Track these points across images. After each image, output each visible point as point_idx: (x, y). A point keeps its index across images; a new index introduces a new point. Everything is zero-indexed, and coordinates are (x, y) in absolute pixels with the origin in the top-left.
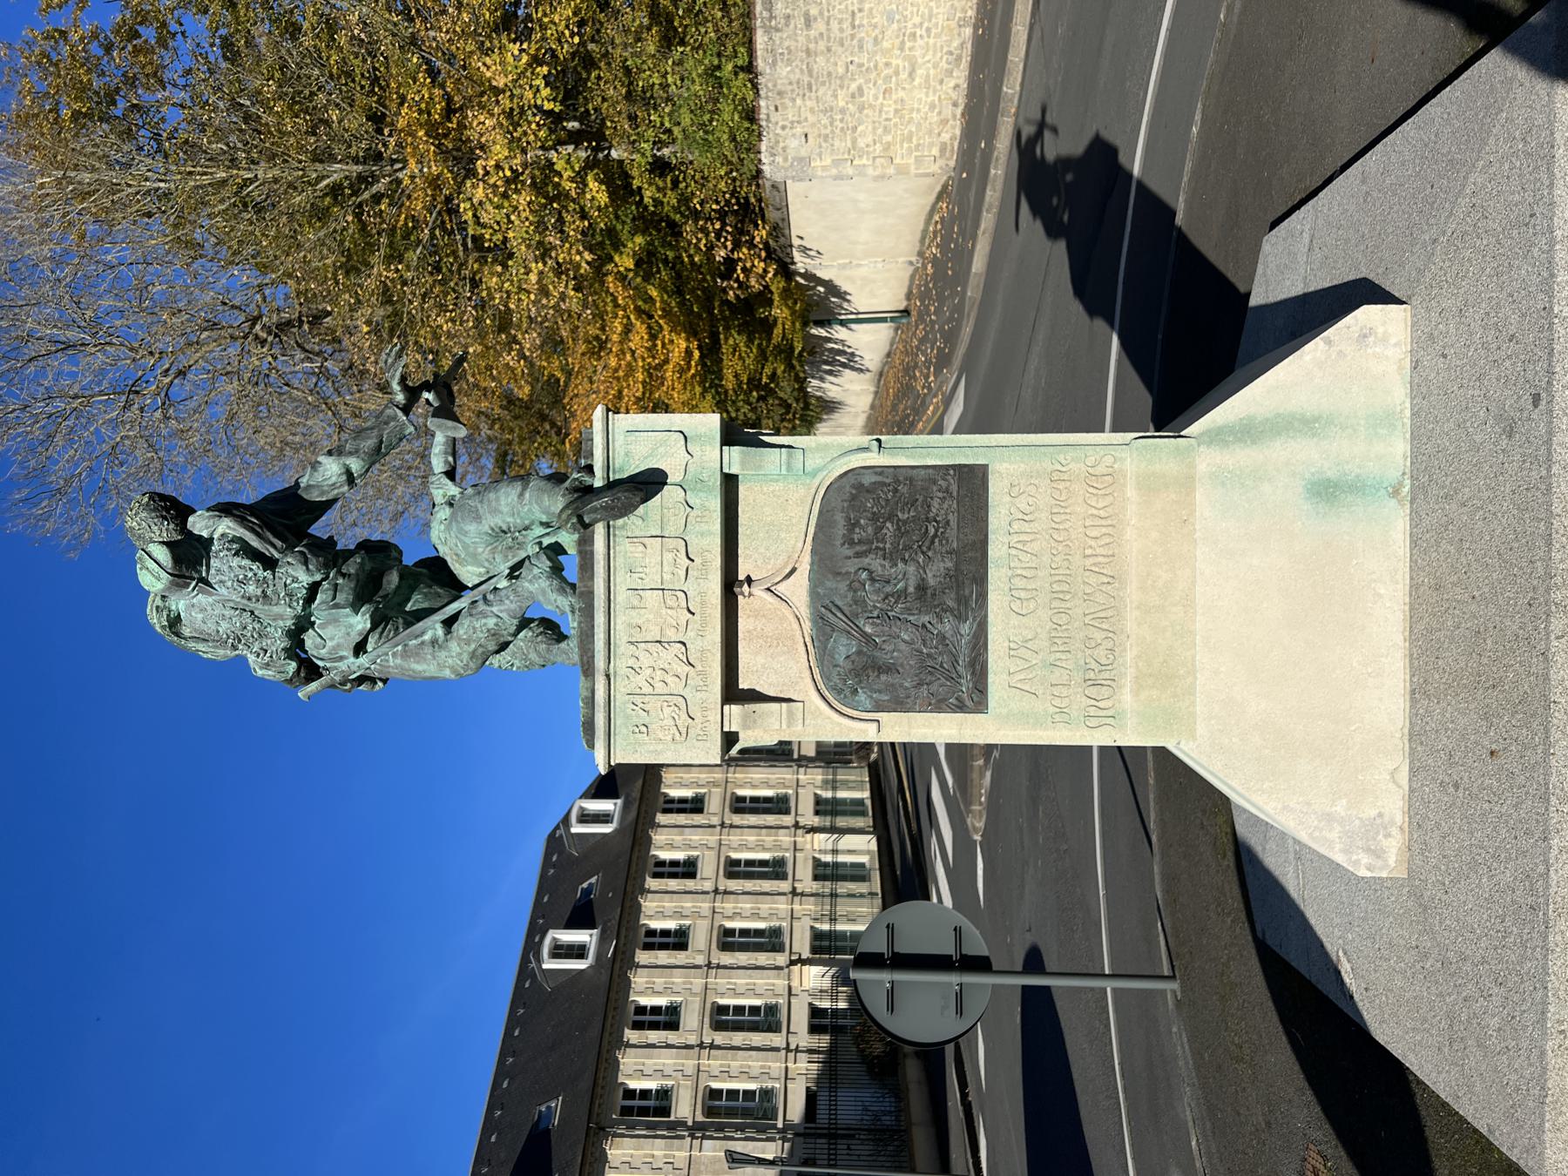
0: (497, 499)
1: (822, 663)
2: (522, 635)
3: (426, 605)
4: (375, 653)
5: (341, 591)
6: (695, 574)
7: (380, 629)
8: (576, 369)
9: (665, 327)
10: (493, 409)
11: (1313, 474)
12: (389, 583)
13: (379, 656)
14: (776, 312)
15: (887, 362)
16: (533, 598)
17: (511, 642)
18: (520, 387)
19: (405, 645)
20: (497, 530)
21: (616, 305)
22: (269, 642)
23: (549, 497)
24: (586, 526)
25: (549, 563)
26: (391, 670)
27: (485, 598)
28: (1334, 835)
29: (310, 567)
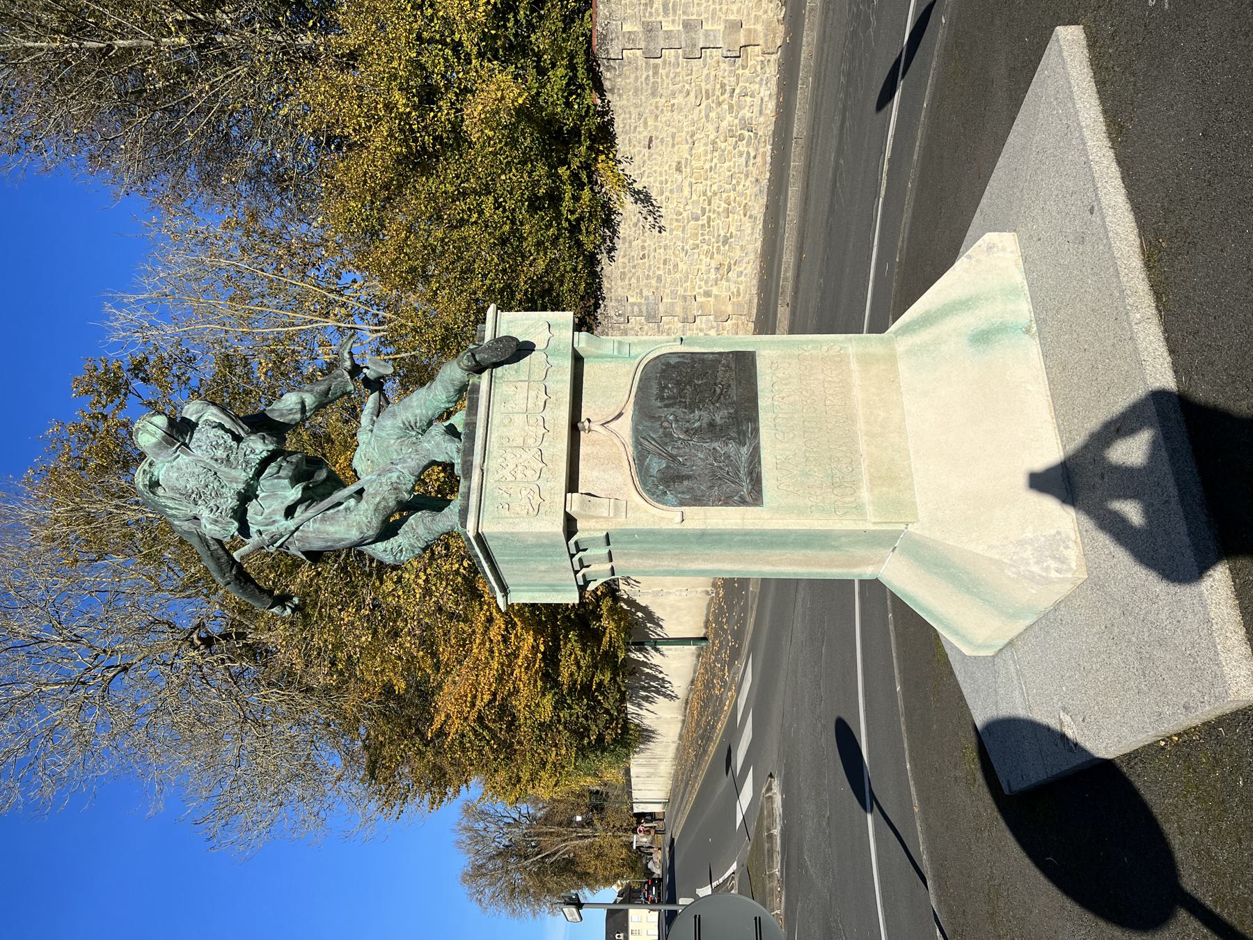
1: (640, 473)
5: (284, 469)
9: (519, 623)
11: (972, 331)
12: (319, 476)
14: (604, 623)
15: (691, 689)
22: (222, 501)
26: (309, 535)
28: (1029, 552)
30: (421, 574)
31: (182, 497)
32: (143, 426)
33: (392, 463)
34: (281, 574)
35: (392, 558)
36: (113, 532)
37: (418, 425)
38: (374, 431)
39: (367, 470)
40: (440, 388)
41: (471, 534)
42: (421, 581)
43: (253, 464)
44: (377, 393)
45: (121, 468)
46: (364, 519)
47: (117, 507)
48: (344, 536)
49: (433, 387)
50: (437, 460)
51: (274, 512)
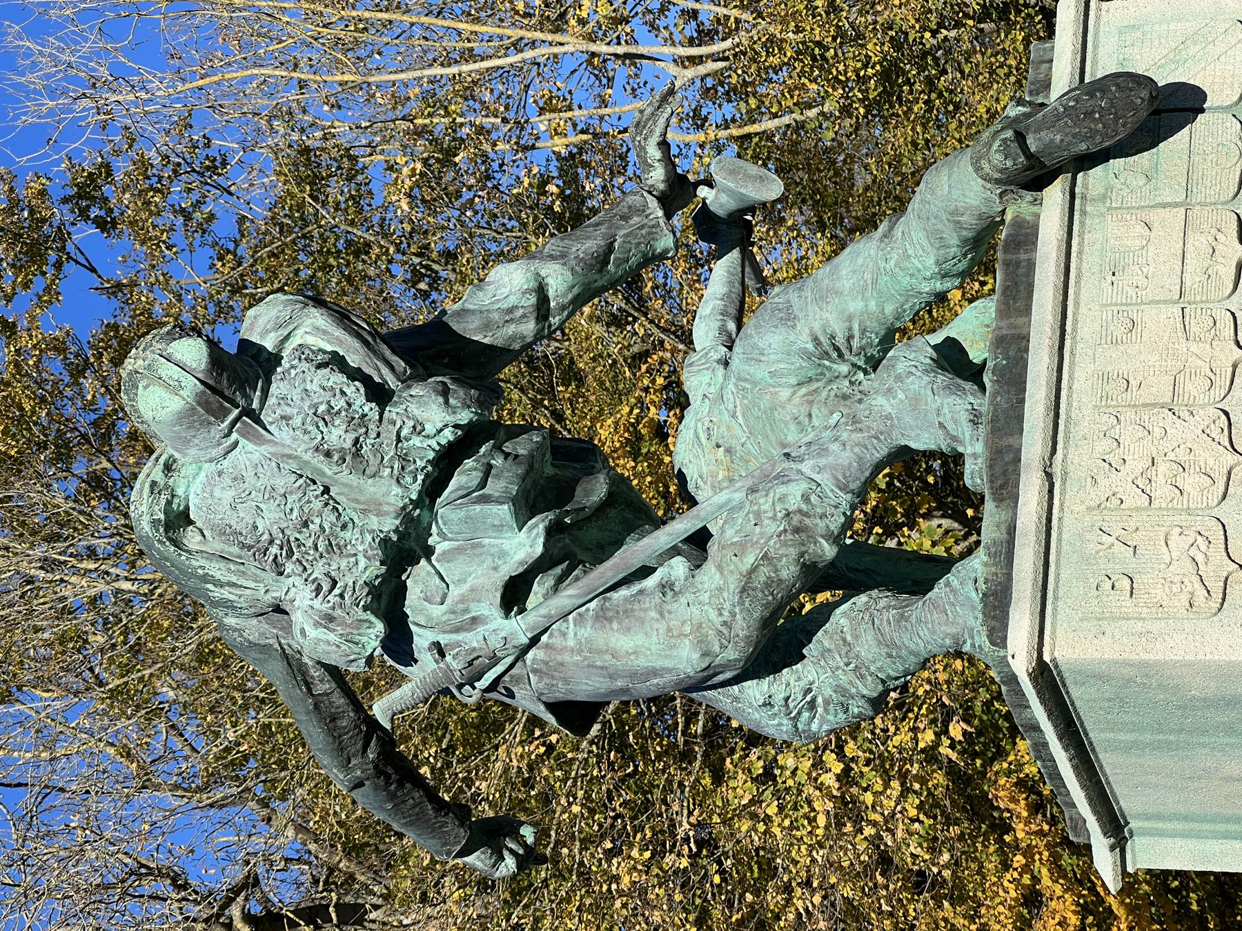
5: (497, 477)
12: (588, 493)
20: (826, 345)
22: (344, 564)
26: (567, 658)
29: (452, 401)
30: (830, 758)
31: (244, 553)
32: (149, 367)
33: (787, 455)
34: (451, 748)
35: (787, 725)
36: (37, 630)
37: (856, 343)
38: (736, 362)
39: (714, 475)
40: (918, 235)
41: (1021, 666)
42: (829, 780)
43: (420, 464)
44: (735, 255)
45: (51, 462)
46: (713, 615)
47: (48, 564)
48: (659, 664)
49: (898, 232)
50: (913, 445)
51: (475, 594)
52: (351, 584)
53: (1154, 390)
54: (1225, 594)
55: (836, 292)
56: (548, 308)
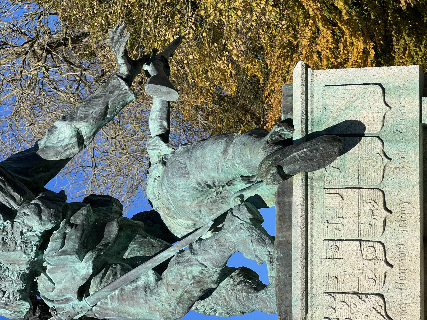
0: (204, 156)
2: (224, 283)
3: (141, 253)
4: (95, 296)
6: (393, 225)
7: (101, 275)
8: (273, 70)
9: (347, 32)
10: (207, 104)
12: (110, 232)
13: (99, 299)
16: (234, 248)
17: (215, 289)
18: (229, 86)
19: (122, 290)
20: (203, 185)
21: (307, 16)
22: (7, 284)
23: (250, 150)
24: (286, 177)
25: (249, 215)
26: (109, 312)
27: (191, 247)
29: (43, 217)
46: (167, 307)
52: (11, 292)
53: (350, 284)
54: (384, 122)
55: (206, 167)
56: (83, 140)
